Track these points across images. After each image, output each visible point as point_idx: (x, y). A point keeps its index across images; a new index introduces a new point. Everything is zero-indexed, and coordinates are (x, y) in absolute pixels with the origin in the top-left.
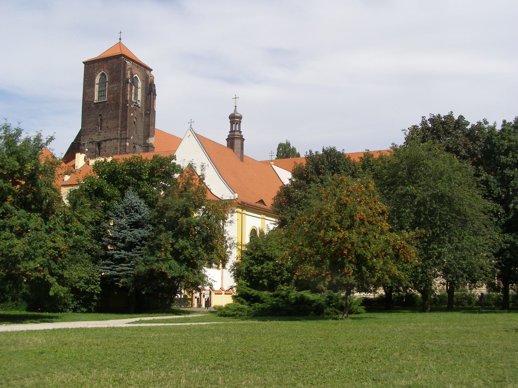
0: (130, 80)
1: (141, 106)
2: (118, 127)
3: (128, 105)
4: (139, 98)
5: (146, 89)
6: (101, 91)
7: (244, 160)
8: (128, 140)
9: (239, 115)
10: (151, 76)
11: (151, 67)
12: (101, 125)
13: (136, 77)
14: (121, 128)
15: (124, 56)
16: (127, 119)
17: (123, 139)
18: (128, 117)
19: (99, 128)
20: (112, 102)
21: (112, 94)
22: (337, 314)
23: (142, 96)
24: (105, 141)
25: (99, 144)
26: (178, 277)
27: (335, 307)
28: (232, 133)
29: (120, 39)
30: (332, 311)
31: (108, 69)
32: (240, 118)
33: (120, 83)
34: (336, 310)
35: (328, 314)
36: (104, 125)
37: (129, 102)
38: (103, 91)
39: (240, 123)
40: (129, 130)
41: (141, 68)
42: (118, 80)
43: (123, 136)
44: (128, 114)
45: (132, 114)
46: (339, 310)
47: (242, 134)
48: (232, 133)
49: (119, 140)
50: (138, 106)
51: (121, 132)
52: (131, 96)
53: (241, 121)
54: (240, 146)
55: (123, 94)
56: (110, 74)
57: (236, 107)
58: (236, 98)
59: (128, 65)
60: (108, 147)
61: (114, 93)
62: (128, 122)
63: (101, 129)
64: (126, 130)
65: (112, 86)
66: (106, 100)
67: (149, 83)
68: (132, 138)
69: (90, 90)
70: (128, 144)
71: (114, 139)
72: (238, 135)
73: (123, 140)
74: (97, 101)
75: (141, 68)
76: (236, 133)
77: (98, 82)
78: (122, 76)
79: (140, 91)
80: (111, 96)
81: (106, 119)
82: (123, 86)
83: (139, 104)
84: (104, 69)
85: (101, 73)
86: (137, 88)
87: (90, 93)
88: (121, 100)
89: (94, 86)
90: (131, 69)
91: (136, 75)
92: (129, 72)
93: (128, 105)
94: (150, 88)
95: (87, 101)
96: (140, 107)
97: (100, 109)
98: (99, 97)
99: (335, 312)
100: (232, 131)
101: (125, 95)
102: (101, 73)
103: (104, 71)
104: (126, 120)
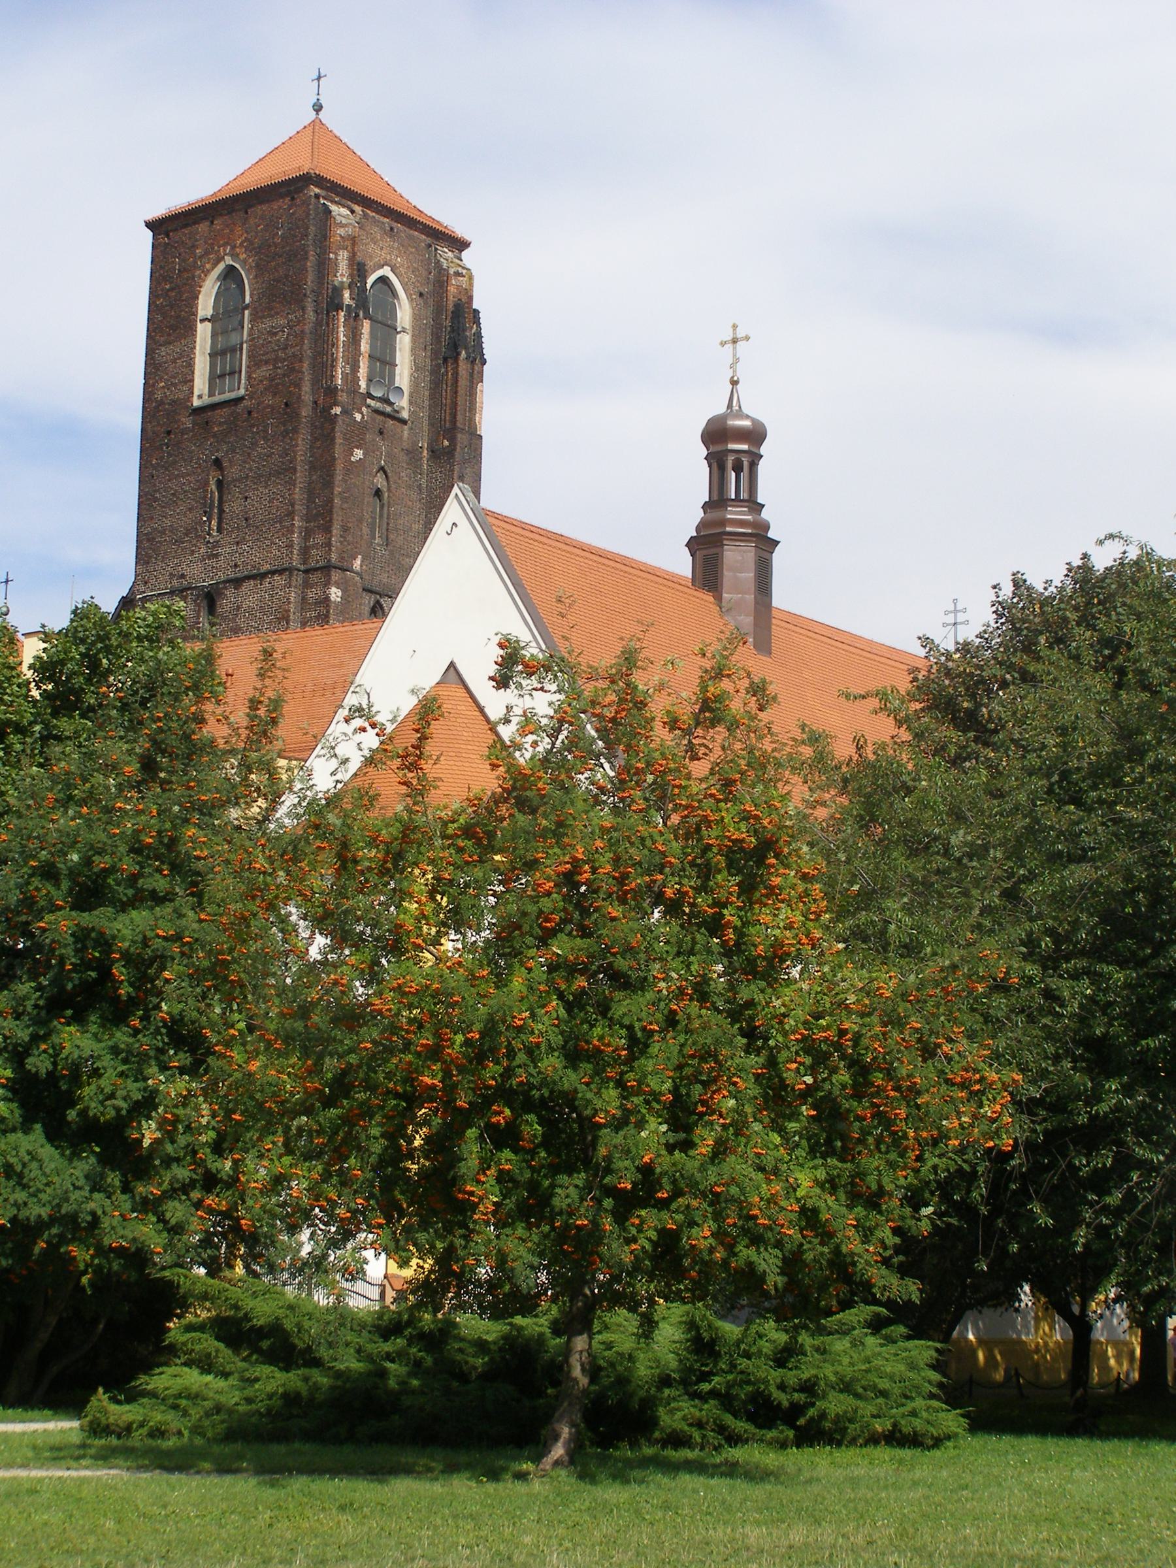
0: (347, 294)
1: (411, 413)
2: (291, 514)
3: (337, 410)
4: (403, 375)
5: (436, 337)
6: (223, 353)
7: (775, 645)
8: (335, 576)
9: (746, 423)
10: (457, 274)
11: (460, 231)
12: (221, 511)
13: (383, 280)
14: (308, 518)
15: (320, 181)
16: (332, 476)
17: (316, 569)
18: (339, 467)
19: (214, 523)
20: (269, 400)
21: (267, 362)
22: (734, 1440)
23: (417, 367)
24: (237, 582)
25: (210, 599)
26: (53, 1220)
27: (725, 1399)
28: (715, 515)
29: (318, 108)
30: (700, 1425)
31: (250, 247)
32: (756, 435)
33: (303, 309)
34: (729, 1420)
35: (677, 1440)
36: (234, 506)
37: (343, 397)
38: (233, 350)
39: (753, 465)
40: (345, 529)
41: (410, 237)
42: (295, 298)
43: (316, 557)
44: (338, 451)
45: (358, 454)
46: (751, 1418)
47: (765, 514)
48: (715, 515)
49: (298, 579)
50: (395, 417)
51: (306, 539)
52: (355, 368)
53: (763, 450)
54: (749, 576)
55: (314, 358)
56: (260, 270)
57: (734, 383)
58: (735, 341)
59: (342, 225)
60: (250, 610)
61: (277, 359)
62: (337, 490)
63: (220, 530)
64: (327, 529)
65: (267, 324)
66: (242, 392)
67: (451, 307)
68: (357, 564)
69: (176, 348)
70: (335, 594)
71: (273, 573)
72: (742, 523)
73: (314, 578)
74: (206, 400)
75: (410, 237)
76: (735, 513)
77: (209, 312)
78: (311, 277)
79: (404, 343)
80: (264, 371)
81: (239, 480)
82: (318, 323)
83: (403, 403)
84: (233, 248)
85: (221, 266)
86: (387, 329)
87: (174, 361)
88: (306, 387)
89: (192, 330)
90: (354, 244)
91: (386, 271)
92: (343, 257)
93: (337, 410)
94: (453, 331)
95: (161, 403)
96: (404, 422)
97: (215, 435)
98: (215, 378)
99: (721, 1429)
100: (716, 502)
101: (323, 366)
102: (221, 266)
103: (234, 256)
104: (329, 484)
